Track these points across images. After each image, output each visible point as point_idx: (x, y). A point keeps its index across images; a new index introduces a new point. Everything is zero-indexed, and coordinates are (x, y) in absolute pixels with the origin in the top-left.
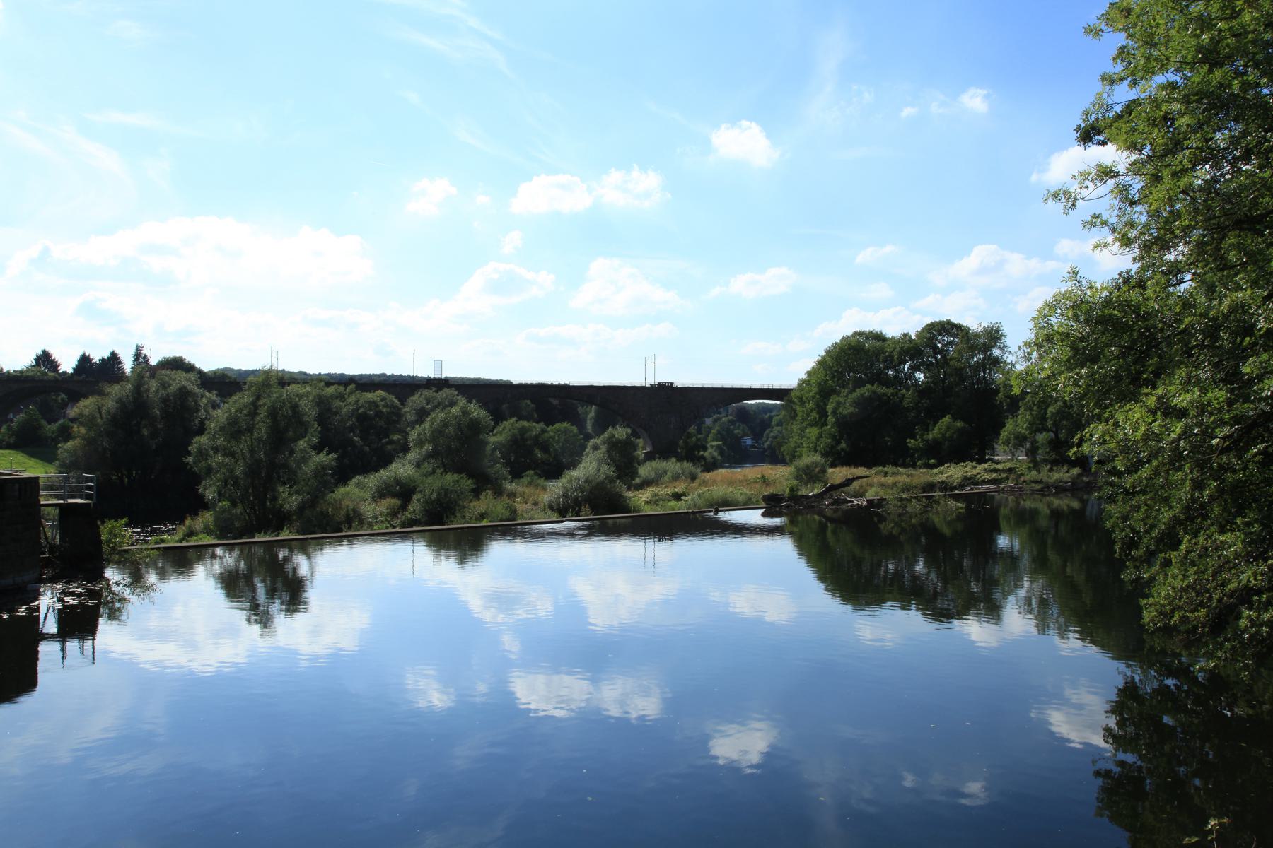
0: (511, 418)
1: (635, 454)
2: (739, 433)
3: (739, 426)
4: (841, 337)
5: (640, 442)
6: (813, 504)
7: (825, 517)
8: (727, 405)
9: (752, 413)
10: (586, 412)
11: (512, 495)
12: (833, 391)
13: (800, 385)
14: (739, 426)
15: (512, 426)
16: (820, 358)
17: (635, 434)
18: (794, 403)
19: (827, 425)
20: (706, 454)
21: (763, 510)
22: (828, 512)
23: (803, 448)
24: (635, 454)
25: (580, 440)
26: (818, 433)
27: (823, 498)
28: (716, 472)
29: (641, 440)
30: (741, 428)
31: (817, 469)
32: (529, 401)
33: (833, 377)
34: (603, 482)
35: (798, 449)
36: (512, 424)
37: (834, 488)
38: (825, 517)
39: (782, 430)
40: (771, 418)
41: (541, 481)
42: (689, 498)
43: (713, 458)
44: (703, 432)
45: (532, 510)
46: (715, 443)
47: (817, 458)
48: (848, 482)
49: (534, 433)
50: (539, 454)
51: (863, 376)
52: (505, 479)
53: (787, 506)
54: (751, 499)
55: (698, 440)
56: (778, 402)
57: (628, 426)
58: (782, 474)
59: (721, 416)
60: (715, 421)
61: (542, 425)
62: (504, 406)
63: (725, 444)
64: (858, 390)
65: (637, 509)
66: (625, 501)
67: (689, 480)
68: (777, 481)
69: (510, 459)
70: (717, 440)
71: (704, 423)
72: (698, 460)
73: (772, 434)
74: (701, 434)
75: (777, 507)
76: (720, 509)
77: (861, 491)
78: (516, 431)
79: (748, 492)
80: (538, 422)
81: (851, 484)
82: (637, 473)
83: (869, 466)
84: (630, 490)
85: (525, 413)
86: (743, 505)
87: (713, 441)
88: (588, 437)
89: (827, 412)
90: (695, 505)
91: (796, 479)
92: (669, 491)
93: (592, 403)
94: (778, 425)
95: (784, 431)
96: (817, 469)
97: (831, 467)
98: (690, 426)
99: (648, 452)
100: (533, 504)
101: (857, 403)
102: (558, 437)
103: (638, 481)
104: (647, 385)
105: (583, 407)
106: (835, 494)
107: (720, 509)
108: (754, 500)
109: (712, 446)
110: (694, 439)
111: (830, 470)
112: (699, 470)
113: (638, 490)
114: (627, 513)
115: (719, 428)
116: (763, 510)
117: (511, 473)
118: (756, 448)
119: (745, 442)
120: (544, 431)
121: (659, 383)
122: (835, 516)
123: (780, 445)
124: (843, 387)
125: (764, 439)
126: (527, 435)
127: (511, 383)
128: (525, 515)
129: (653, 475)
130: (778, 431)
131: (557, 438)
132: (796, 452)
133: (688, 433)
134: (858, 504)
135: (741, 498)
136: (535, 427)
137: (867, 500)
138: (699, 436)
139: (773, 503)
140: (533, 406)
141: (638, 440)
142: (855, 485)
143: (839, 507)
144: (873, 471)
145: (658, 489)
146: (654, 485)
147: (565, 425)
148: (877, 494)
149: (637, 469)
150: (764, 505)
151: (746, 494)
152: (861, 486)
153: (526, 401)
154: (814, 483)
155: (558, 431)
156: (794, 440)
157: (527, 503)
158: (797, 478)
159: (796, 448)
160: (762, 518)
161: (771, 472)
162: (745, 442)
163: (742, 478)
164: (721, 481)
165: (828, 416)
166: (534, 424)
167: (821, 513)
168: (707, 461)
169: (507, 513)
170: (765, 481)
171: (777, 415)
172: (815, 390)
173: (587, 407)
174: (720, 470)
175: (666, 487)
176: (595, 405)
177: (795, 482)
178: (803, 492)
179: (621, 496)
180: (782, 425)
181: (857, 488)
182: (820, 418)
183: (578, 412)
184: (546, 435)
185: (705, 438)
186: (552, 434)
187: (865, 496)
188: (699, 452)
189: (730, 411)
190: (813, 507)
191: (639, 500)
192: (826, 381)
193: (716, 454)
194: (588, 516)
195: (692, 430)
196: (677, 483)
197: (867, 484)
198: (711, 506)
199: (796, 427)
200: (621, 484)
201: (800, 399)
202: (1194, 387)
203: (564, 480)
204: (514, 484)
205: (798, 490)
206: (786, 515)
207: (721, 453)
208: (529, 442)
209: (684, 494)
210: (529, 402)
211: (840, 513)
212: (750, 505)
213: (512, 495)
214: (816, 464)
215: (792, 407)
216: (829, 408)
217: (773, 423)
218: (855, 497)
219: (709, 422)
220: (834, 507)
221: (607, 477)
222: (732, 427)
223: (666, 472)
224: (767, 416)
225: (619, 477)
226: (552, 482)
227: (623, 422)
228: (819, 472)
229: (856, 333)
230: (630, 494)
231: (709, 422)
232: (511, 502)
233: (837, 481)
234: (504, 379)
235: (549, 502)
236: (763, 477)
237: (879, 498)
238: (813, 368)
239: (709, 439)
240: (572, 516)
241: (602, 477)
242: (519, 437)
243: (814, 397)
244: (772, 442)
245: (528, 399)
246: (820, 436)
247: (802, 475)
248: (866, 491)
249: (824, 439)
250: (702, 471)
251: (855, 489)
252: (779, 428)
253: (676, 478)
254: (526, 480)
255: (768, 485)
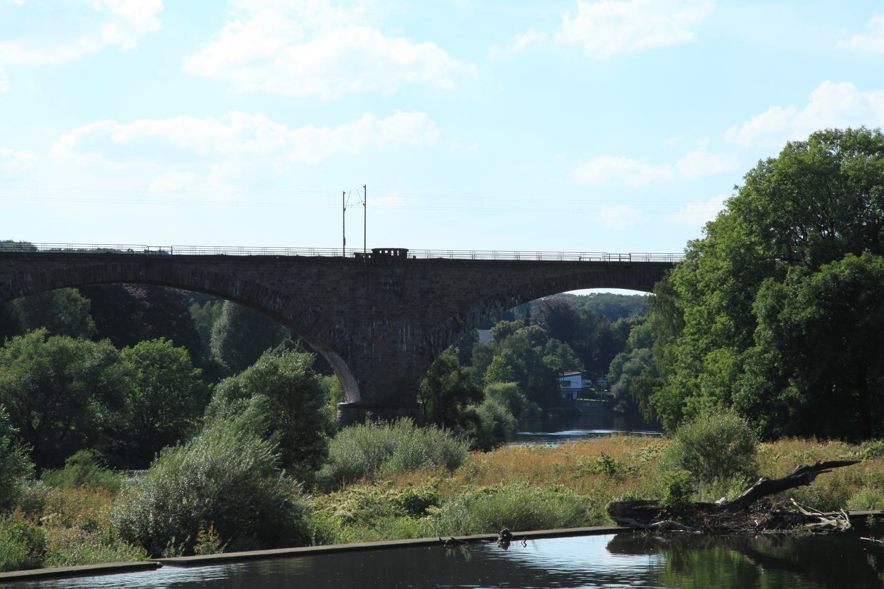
0: (32, 330)
1: (322, 410)
2: (552, 362)
3: (555, 347)
4: (785, 145)
5: (332, 382)
6: (725, 524)
7: (753, 554)
8: (527, 300)
9: (584, 317)
10: (211, 316)
11: (34, 508)
12: (766, 269)
13: (692, 255)
14: (555, 347)
15: (36, 347)
16: (737, 194)
17: (321, 366)
18: (678, 295)
19: (753, 344)
20: (480, 410)
21: (611, 537)
22: (762, 543)
23: (699, 395)
24: (322, 410)
25: (195, 377)
26: (735, 364)
27: (748, 511)
28: (502, 451)
29: (335, 377)
30: (559, 351)
31: (732, 445)
32: (75, 290)
33: (767, 236)
34: (247, 475)
35: (687, 399)
36: (36, 343)
37: (773, 487)
38: (753, 554)
39: (651, 356)
40: (626, 329)
41: (107, 476)
42: (446, 508)
43: (497, 418)
44: (474, 359)
45: (82, 541)
46: (500, 386)
47: (731, 419)
48: (805, 475)
49: (87, 364)
50: (98, 411)
51: (836, 234)
52: (20, 471)
53: (667, 529)
54: (584, 511)
55: (463, 377)
56: (642, 294)
57: (306, 348)
58: (654, 454)
59: (512, 324)
60: (502, 335)
61: (106, 345)
62: (15, 302)
63: (522, 386)
64: (824, 267)
65: (325, 535)
66: (299, 518)
67: (442, 469)
68: (641, 472)
69: (30, 424)
70: (505, 379)
71: (474, 339)
72: (464, 425)
73: (628, 365)
74: (470, 364)
75: (643, 529)
76: (514, 534)
77: (836, 495)
78: (46, 360)
79: (576, 495)
80: (96, 339)
81: (813, 479)
82: (326, 455)
83: (853, 440)
84: (310, 492)
85: (64, 317)
86: (565, 526)
87: (496, 379)
88: (214, 373)
89: (754, 317)
90: (458, 525)
91: (686, 468)
92: (397, 493)
93: (223, 295)
94: (641, 344)
95: (655, 359)
96: (732, 445)
97: (763, 441)
98: (445, 347)
99: (349, 405)
100: (85, 528)
101: (817, 296)
102: (143, 372)
103: (326, 471)
104: (347, 256)
105: (202, 305)
106: (775, 502)
107: (514, 534)
108: (591, 514)
109: (493, 392)
110: (454, 375)
111: (763, 447)
112: (464, 447)
113: (327, 492)
114: (548, 528)
115: (509, 352)
116: (611, 537)
117: (34, 457)
118: (591, 395)
119: (569, 383)
120: (110, 359)
121: (376, 251)
122: (775, 552)
123: (648, 389)
124: (792, 260)
125: (610, 376)
126: (71, 369)
127: (34, 248)
128: (64, 553)
129: (359, 457)
130: (642, 359)
131: (140, 375)
132: (685, 405)
133: (442, 363)
134: (829, 526)
135: (561, 511)
136: (90, 351)
137: (852, 518)
138: (465, 369)
139: (633, 522)
140: (84, 300)
141: (327, 378)
142: (822, 481)
143: (785, 532)
144: (863, 449)
145: (374, 489)
146: (363, 480)
147: (160, 344)
148: (872, 503)
149: (324, 444)
150: (613, 525)
151: (571, 501)
152: (835, 485)
153: (69, 290)
154: (727, 475)
155: (144, 357)
156: (675, 382)
157: (69, 526)
158: (686, 463)
159: (683, 396)
160: (608, 555)
161: (626, 450)
162: (569, 383)
163: (562, 463)
164: (516, 470)
165: (757, 324)
166: (88, 342)
167: (746, 548)
168: (484, 424)
169: (22, 551)
170: (611, 470)
171: (641, 323)
172: (725, 264)
173: (212, 305)
174: (512, 446)
175: (391, 485)
176: (230, 299)
177: (685, 474)
178: (702, 495)
179: (288, 505)
180: (650, 345)
181: (826, 488)
182: (737, 328)
183: (189, 315)
184: (115, 370)
185: (480, 374)
186: (131, 366)
187: (845, 505)
188: (464, 405)
189: (534, 312)
190: (725, 530)
191: (329, 515)
192: (750, 248)
193: (502, 409)
194: (213, 553)
195: (448, 355)
196: (417, 475)
197: (849, 481)
198: (495, 527)
199: (682, 349)
200: (290, 478)
201: (692, 285)
202: (779, 321)
203: (160, 470)
204: (40, 483)
205: (690, 491)
206: (665, 547)
207: (515, 407)
208: (76, 385)
209: (433, 501)
210: (75, 292)
211: (787, 547)
212: (538, 528)
213: (34, 508)
214: (729, 434)
215: (672, 303)
216: (759, 307)
217: (631, 340)
218: (821, 508)
219: (485, 337)
220: (774, 531)
221: (259, 464)
222: (538, 349)
223: (389, 450)
224: (616, 325)
225: (285, 463)
226: (131, 475)
227: (294, 338)
228: (736, 452)
229: (817, 138)
230: (308, 501)
231: (485, 337)
232: (32, 525)
233: (780, 473)
234: (16, 240)
235: (123, 521)
236: (608, 463)
237: (878, 512)
238: (721, 216)
239: (488, 375)
240: (176, 555)
241: (247, 462)
242: (51, 372)
243: (724, 281)
244: (629, 383)
245: (73, 287)
246: (739, 369)
247: (697, 458)
248: (846, 496)
249: (748, 375)
250: (473, 448)
251: (821, 489)
252: (644, 351)
253: (413, 463)
254: (70, 472)
255: (620, 480)
